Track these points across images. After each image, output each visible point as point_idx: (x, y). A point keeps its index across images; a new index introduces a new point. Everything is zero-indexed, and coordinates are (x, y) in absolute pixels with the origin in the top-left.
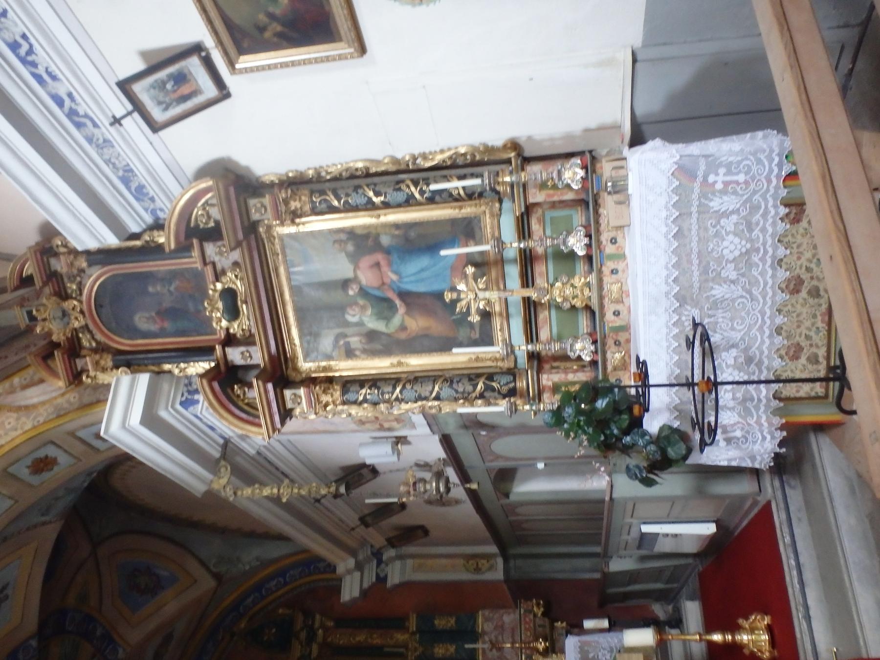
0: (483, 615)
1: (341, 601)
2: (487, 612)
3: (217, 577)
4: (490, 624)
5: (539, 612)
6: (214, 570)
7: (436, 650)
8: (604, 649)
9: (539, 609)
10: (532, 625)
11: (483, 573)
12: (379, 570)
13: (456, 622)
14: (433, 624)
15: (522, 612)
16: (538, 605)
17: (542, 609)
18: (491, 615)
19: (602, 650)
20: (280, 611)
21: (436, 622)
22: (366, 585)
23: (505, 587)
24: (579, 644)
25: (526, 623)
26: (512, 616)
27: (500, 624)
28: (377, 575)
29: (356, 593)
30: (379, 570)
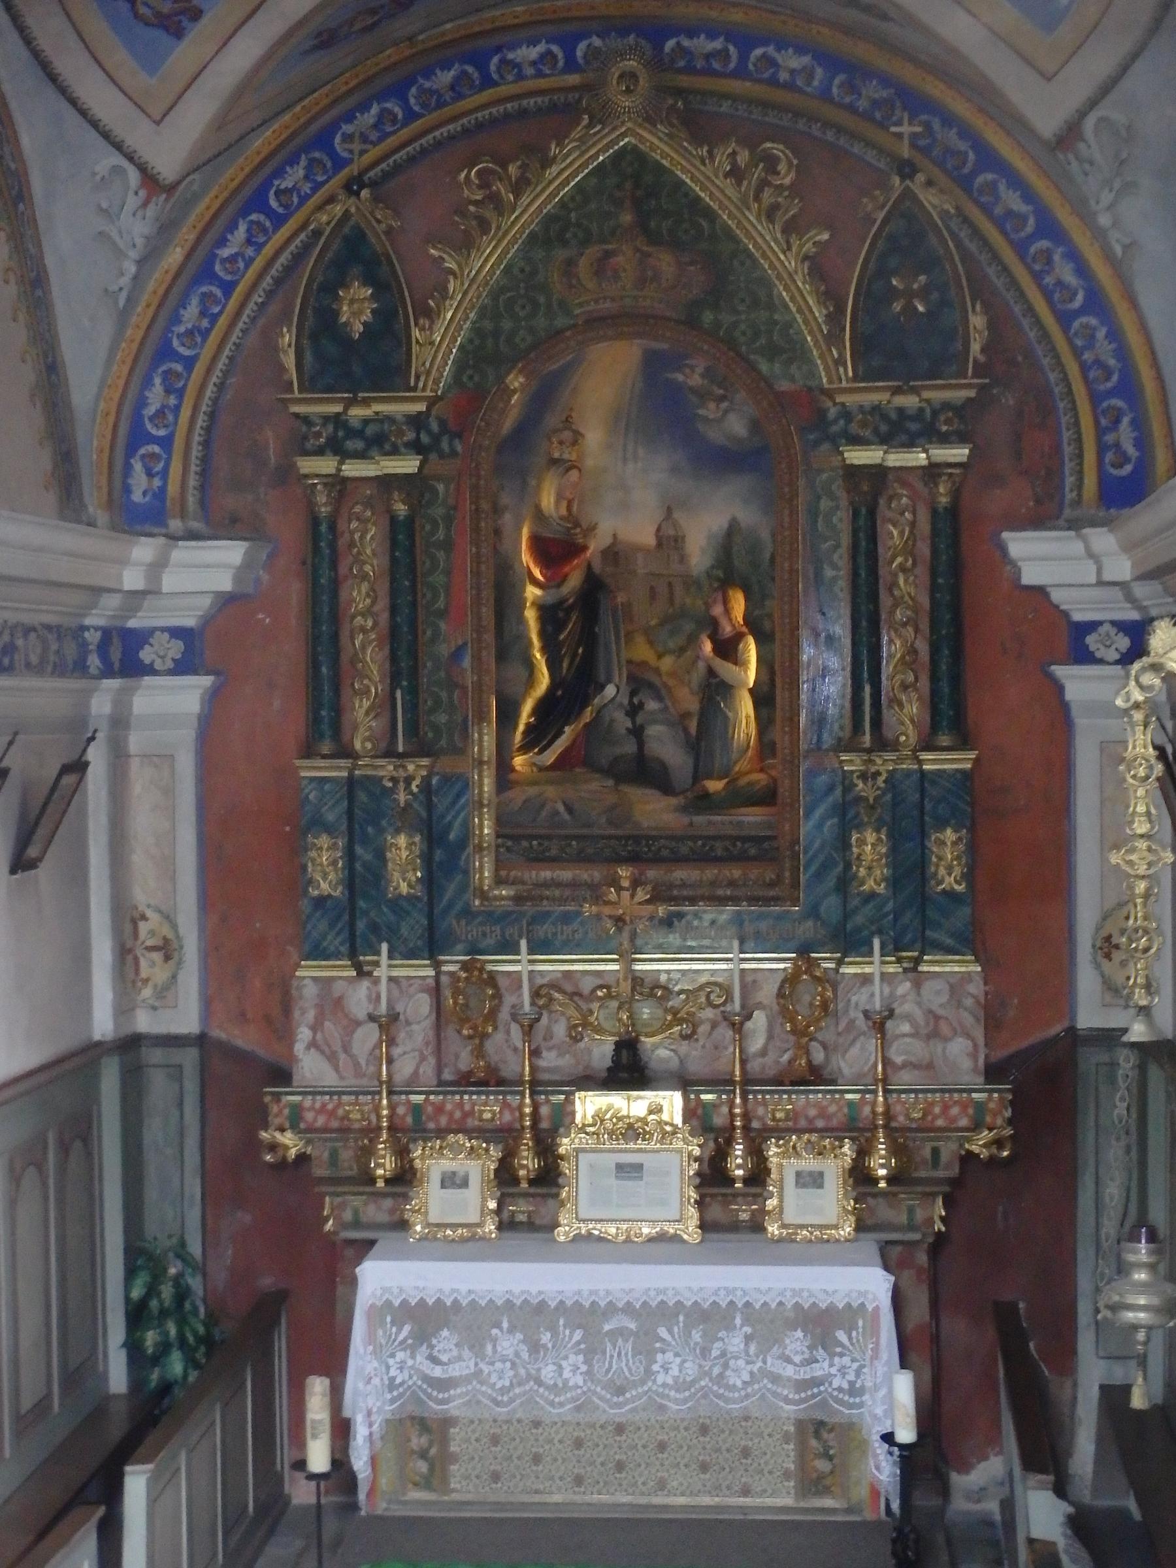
0: (967, 977)
1: (1005, 535)
2: (976, 988)
3: (1069, 136)
4: (944, 998)
5: (979, 1144)
6: (1089, 123)
7: (870, 836)
8: (858, 1373)
9: (985, 1146)
10: (940, 1122)
11: (1098, 966)
12: (1106, 627)
13: (949, 894)
14: (941, 824)
15: (974, 1095)
16: (999, 1143)
17: (984, 1154)
18: (969, 1002)
19: (855, 1365)
20: (977, 321)
21: (949, 835)
22: (1056, 596)
23: (1056, 1029)
24: (870, 1307)
25: (946, 1108)
26: (966, 1064)
27: (945, 1029)
28: (1093, 626)
29: (1031, 576)
30: (1106, 627)
